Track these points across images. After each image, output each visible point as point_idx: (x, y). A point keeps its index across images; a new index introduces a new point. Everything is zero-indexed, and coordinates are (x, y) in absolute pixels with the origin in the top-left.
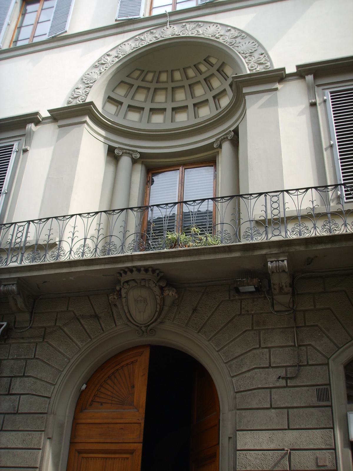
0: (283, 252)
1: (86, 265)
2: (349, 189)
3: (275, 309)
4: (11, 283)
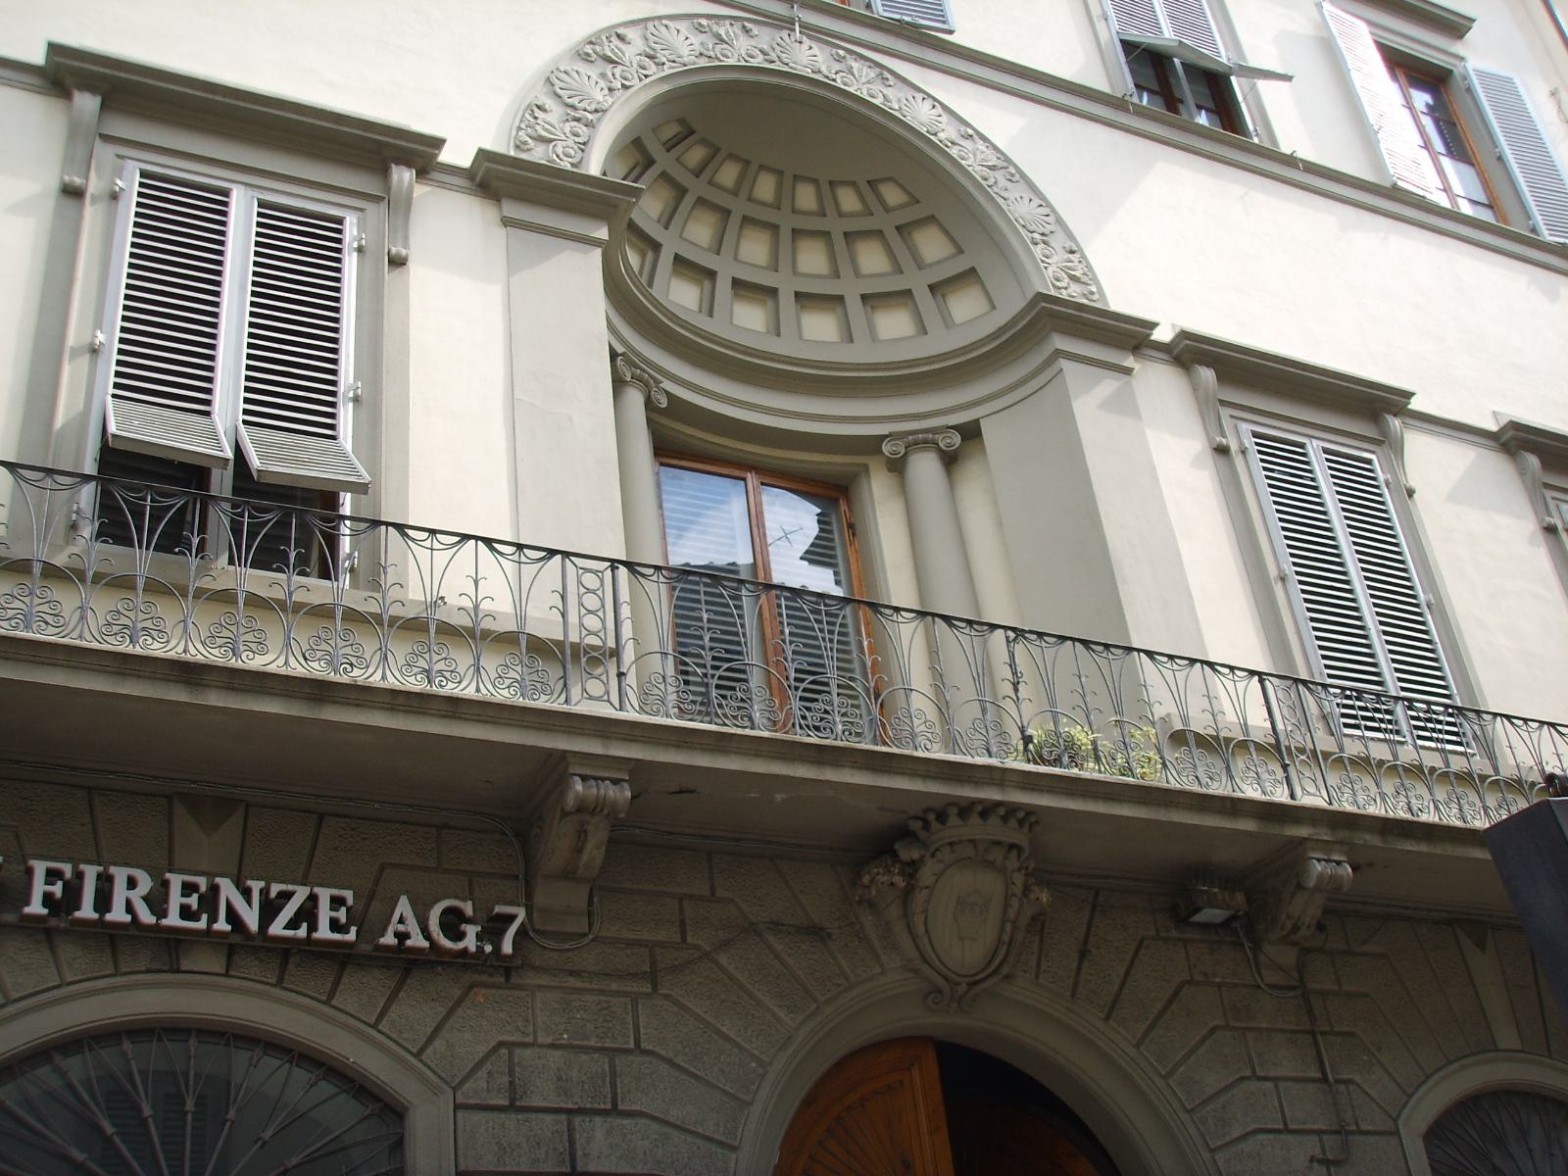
0: (1340, 843)
1: (867, 769)
2: (1421, 715)
3: (1265, 978)
4: (607, 775)
